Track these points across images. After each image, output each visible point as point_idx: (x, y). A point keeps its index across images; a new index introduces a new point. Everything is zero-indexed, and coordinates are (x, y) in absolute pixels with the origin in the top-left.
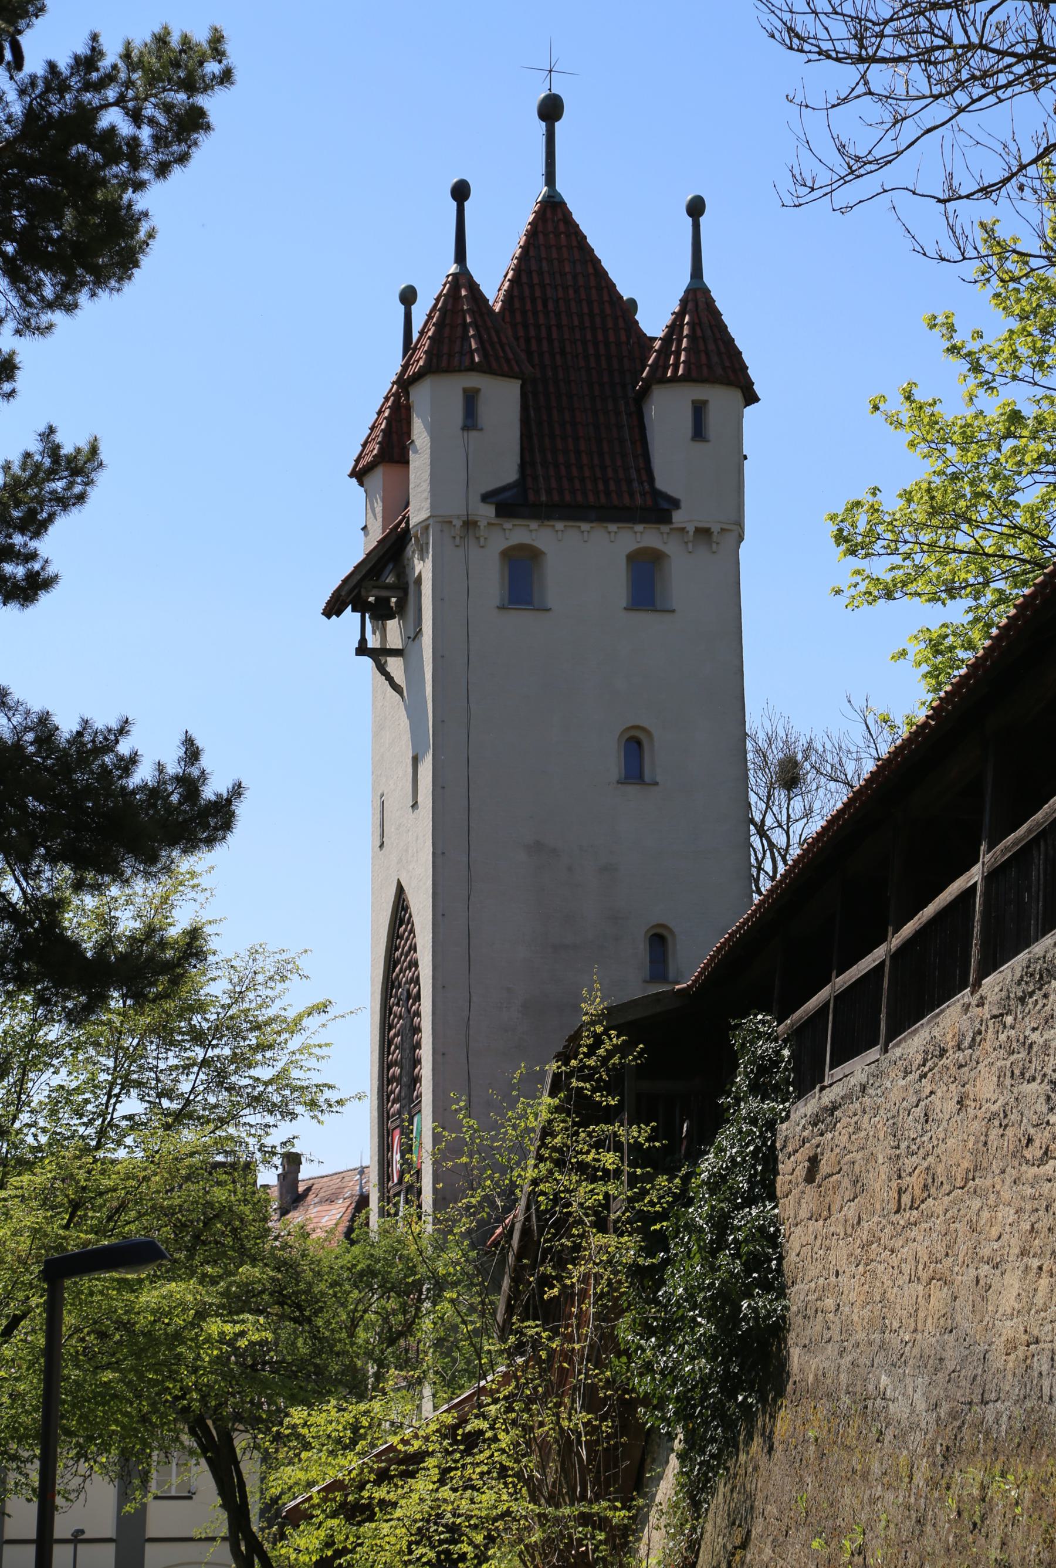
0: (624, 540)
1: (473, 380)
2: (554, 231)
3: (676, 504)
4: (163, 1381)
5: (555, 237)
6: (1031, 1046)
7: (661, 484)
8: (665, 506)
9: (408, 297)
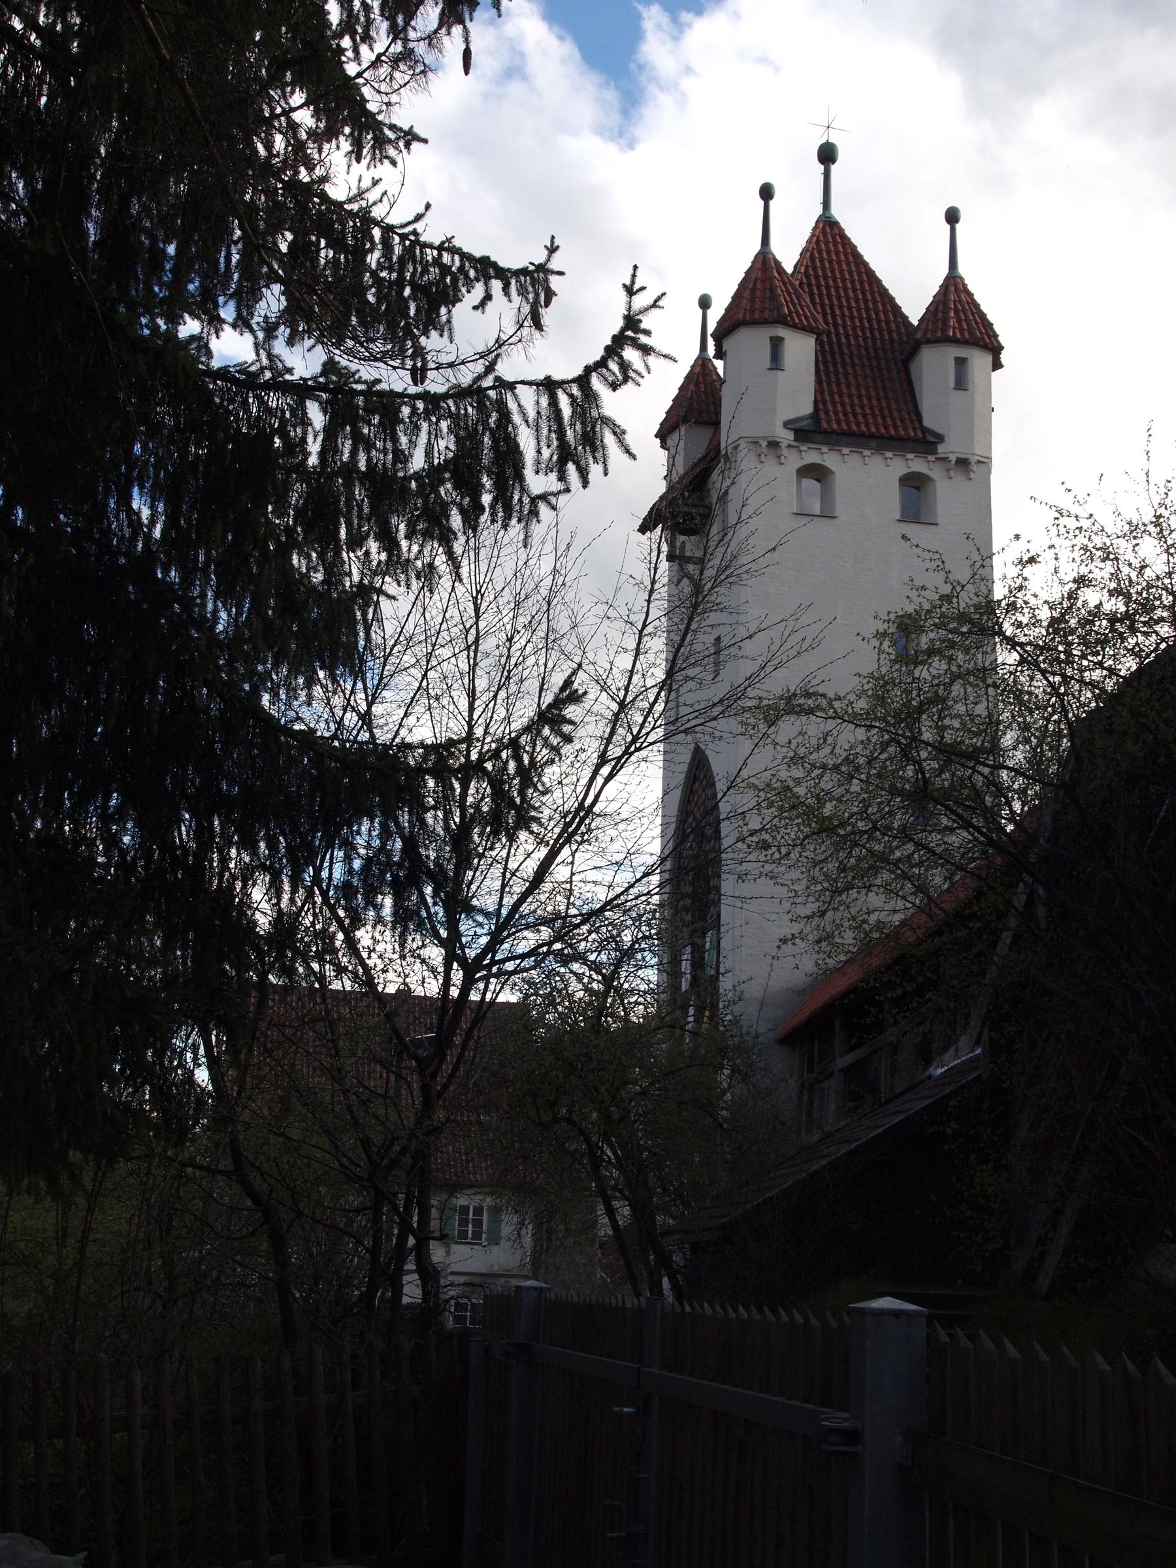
0: (896, 466)
1: (781, 332)
3: (940, 438)
4: (491, 430)
7: (927, 423)
8: (933, 440)
9: (705, 303)
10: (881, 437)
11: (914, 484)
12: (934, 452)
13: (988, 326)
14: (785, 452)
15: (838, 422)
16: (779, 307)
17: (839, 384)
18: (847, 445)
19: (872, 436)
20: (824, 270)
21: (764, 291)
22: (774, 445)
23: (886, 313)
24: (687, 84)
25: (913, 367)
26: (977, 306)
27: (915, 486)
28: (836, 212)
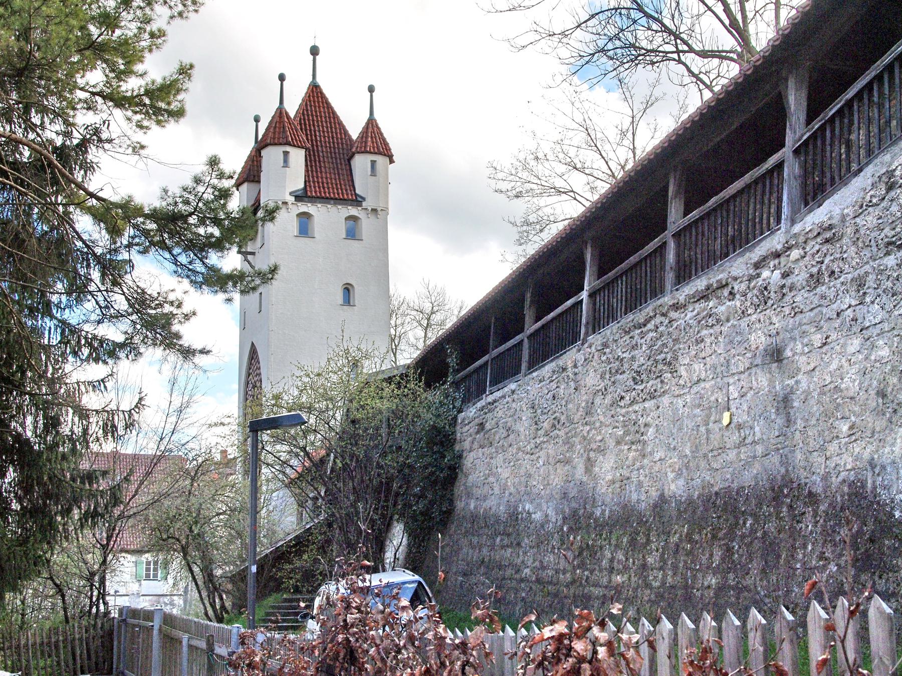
1: (288, 148)
2: (315, 94)
5: (315, 95)
6: (622, 360)
9: (257, 120)
10: (336, 199)
12: (361, 206)
13: (386, 144)
14: (290, 206)
15: (316, 192)
16: (287, 137)
17: (317, 172)
18: (320, 203)
19: (332, 199)
20: (312, 111)
21: (280, 128)
23: (341, 134)
25: (352, 163)
26: (382, 134)
28: (320, 81)
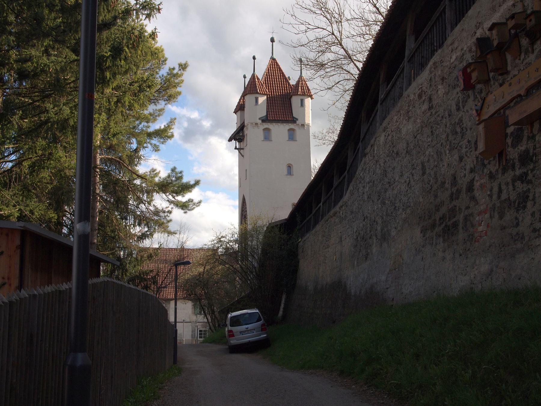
1: (257, 95)
7: (294, 116)
11: (291, 131)
14: (259, 125)
22: (256, 124)
24: (178, 170)
27: (291, 132)
